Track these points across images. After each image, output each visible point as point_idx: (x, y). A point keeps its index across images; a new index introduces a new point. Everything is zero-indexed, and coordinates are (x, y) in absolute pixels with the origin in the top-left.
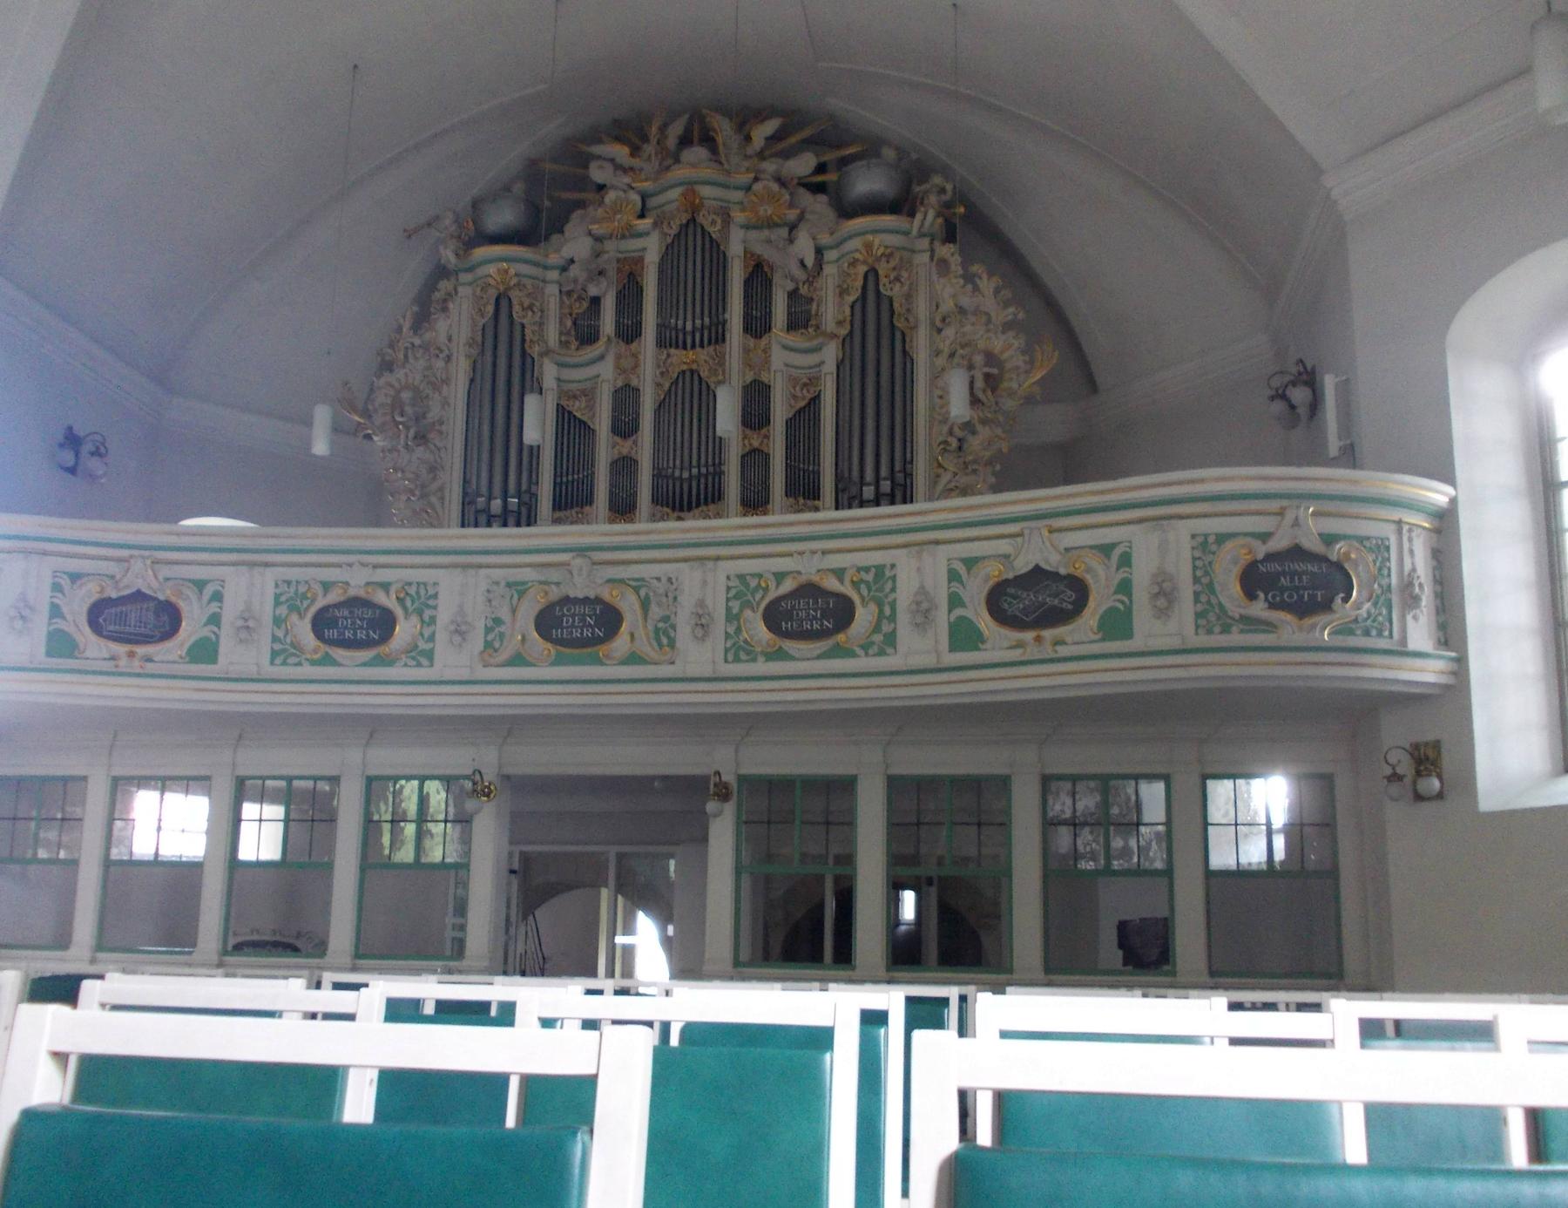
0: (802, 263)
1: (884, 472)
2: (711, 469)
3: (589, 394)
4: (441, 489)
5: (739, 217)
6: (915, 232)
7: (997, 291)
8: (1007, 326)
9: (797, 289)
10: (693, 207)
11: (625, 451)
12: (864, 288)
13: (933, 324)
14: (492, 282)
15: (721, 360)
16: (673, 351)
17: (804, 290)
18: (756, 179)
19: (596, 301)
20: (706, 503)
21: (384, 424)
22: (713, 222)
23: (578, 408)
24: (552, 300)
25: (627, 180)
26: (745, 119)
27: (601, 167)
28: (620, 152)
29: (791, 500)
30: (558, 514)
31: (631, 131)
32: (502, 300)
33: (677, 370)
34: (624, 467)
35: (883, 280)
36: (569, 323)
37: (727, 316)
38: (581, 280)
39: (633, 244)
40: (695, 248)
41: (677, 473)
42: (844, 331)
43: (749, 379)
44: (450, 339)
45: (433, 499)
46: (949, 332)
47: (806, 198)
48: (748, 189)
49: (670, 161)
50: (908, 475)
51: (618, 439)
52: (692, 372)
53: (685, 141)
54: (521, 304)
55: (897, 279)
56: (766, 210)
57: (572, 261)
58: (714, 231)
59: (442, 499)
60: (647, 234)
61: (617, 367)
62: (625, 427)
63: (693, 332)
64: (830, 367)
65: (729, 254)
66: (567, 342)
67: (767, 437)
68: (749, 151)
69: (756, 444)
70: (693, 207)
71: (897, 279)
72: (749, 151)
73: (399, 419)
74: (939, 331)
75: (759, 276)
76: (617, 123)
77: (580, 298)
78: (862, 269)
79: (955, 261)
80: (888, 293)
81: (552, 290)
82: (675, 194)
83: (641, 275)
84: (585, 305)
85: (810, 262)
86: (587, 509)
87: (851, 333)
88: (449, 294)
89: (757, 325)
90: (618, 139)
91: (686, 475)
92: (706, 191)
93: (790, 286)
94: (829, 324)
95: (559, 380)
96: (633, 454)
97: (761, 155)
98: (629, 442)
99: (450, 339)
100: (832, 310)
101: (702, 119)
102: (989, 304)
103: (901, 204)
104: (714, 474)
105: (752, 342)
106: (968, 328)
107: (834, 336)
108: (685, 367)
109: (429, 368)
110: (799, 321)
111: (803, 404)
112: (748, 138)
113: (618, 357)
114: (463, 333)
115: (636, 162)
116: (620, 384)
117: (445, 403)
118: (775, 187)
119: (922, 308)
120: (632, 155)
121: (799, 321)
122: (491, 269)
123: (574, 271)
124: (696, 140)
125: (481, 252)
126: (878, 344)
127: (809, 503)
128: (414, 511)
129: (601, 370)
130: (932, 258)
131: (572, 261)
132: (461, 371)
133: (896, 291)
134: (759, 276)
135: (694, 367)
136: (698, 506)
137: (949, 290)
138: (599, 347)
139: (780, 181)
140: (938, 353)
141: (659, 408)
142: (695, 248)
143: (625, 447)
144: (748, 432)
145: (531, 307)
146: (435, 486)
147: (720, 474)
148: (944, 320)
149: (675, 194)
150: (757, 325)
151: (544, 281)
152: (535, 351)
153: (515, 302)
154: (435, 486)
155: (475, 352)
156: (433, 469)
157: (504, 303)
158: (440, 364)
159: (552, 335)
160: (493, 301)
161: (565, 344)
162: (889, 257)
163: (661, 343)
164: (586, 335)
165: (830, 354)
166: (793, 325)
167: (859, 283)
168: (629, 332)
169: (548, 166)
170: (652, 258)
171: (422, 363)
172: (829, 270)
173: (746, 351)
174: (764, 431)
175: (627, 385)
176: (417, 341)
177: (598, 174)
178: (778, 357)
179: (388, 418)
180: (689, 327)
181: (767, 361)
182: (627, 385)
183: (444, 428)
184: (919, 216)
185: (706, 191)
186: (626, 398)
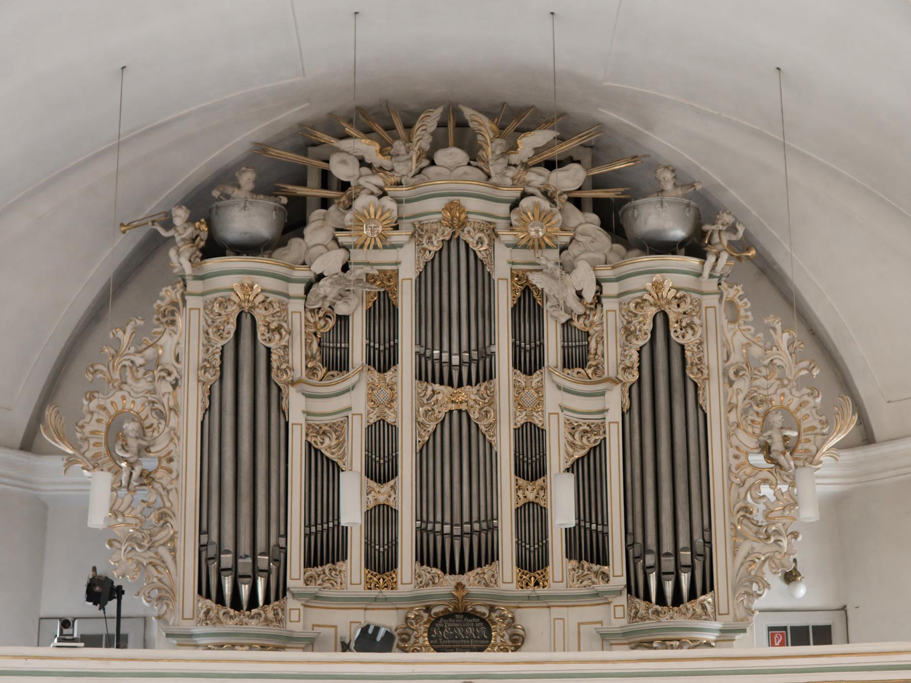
0: (579, 294)
1: (473, 346)
2: (484, 525)
3: (338, 429)
4: (172, 539)
5: (507, 236)
6: (706, 273)
7: (791, 343)
8: (803, 382)
9: (571, 320)
10: (456, 219)
11: (382, 499)
12: (653, 332)
13: (725, 373)
14: (234, 298)
15: (490, 401)
16: (437, 387)
17: (578, 324)
18: (524, 195)
19: (343, 320)
20: (480, 565)
21: (95, 456)
22: (480, 241)
23: (326, 446)
24: (296, 317)
25: (377, 180)
26: (514, 119)
27: (344, 162)
28: (368, 148)
29: (574, 563)
30: (312, 571)
31: (384, 120)
32: (245, 320)
33: (445, 410)
34: (381, 518)
35: (674, 326)
36: (315, 346)
37: (494, 349)
38: (330, 298)
39: (388, 256)
40: (455, 270)
41: (438, 527)
42: (633, 377)
43: (521, 419)
44: (177, 359)
45: (163, 551)
46: (742, 385)
47: (576, 217)
48: (515, 205)
49: (426, 162)
50: (708, 543)
51: (373, 484)
52: (460, 411)
53: (438, 143)
54: (268, 326)
55: (690, 326)
56: (536, 231)
57: (320, 277)
58: (481, 250)
59: (173, 550)
60: (401, 246)
61: (371, 399)
62: (381, 469)
63: (460, 366)
64: (614, 415)
65: (495, 277)
66: (314, 368)
67: (543, 488)
68: (514, 158)
69: (531, 496)
70: (456, 219)
71: (690, 326)
72: (514, 158)
73: (121, 453)
74: (731, 383)
75: (528, 305)
76: (360, 110)
77: (326, 316)
78: (651, 311)
79: (744, 306)
80: (681, 341)
81: (297, 306)
82: (437, 204)
83: (395, 293)
84: (331, 323)
85: (589, 296)
86: (339, 565)
87: (640, 380)
88: (174, 303)
89: (528, 360)
90: (367, 132)
91: (457, 531)
92: (471, 204)
93: (564, 318)
94: (611, 367)
95: (308, 413)
96: (391, 503)
97: (526, 166)
98: (386, 488)
99: (177, 359)
100: (613, 352)
101: (457, 112)
102: (783, 357)
103: (695, 246)
104: (489, 528)
105: (522, 378)
106: (761, 382)
107: (616, 381)
108: (453, 407)
109: (153, 392)
110: (577, 357)
111: (583, 452)
112: (514, 148)
113: (372, 388)
114: (195, 355)
115: (386, 162)
116: (373, 419)
117: (174, 436)
118: (546, 205)
119: (713, 358)
120: (382, 152)
121: (577, 357)
122: (232, 281)
123: (324, 287)
124: (451, 141)
125: (214, 264)
126: (665, 381)
127: (595, 567)
128: (139, 563)
129: (353, 400)
130: (720, 300)
131: (320, 277)
132: (192, 401)
133: (690, 340)
134: (528, 305)
135: (464, 407)
136: (471, 568)
137: (739, 339)
138: (351, 378)
139: (547, 194)
140: (731, 407)
141: (421, 453)
142: (455, 270)
143: (382, 494)
144: (521, 482)
145: (278, 329)
146: (163, 535)
147: (493, 529)
148: (736, 373)
149: (437, 204)
150: (528, 360)
151: (287, 296)
152: (279, 379)
153: (260, 323)
154: (163, 535)
155: (211, 377)
156: (164, 517)
157: (246, 323)
158: (165, 387)
159: (297, 359)
160: (233, 320)
161: (312, 371)
162: (680, 300)
163: (421, 375)
164: (337, 363)
165: (614, 402)
166: (568, 363)
167: (648, 327)
168: (383, 359)
169: (274, 152)
170: (408, 273)
171: (143, 385)
172: (607, 304)
173: (519, 389)
174: (540, 482)
175: (382, 421)
176: (139, 360)
177: (341, 170)
178: (553, 399)
179: (103, 449)
180: (455, 360)
181: (540, 402)
182: (382, 421)
183: (173, 465)
184: (711, 259)
185: (471, 204)
186: (381, 436)
